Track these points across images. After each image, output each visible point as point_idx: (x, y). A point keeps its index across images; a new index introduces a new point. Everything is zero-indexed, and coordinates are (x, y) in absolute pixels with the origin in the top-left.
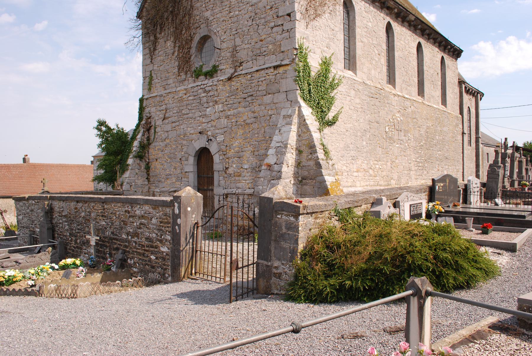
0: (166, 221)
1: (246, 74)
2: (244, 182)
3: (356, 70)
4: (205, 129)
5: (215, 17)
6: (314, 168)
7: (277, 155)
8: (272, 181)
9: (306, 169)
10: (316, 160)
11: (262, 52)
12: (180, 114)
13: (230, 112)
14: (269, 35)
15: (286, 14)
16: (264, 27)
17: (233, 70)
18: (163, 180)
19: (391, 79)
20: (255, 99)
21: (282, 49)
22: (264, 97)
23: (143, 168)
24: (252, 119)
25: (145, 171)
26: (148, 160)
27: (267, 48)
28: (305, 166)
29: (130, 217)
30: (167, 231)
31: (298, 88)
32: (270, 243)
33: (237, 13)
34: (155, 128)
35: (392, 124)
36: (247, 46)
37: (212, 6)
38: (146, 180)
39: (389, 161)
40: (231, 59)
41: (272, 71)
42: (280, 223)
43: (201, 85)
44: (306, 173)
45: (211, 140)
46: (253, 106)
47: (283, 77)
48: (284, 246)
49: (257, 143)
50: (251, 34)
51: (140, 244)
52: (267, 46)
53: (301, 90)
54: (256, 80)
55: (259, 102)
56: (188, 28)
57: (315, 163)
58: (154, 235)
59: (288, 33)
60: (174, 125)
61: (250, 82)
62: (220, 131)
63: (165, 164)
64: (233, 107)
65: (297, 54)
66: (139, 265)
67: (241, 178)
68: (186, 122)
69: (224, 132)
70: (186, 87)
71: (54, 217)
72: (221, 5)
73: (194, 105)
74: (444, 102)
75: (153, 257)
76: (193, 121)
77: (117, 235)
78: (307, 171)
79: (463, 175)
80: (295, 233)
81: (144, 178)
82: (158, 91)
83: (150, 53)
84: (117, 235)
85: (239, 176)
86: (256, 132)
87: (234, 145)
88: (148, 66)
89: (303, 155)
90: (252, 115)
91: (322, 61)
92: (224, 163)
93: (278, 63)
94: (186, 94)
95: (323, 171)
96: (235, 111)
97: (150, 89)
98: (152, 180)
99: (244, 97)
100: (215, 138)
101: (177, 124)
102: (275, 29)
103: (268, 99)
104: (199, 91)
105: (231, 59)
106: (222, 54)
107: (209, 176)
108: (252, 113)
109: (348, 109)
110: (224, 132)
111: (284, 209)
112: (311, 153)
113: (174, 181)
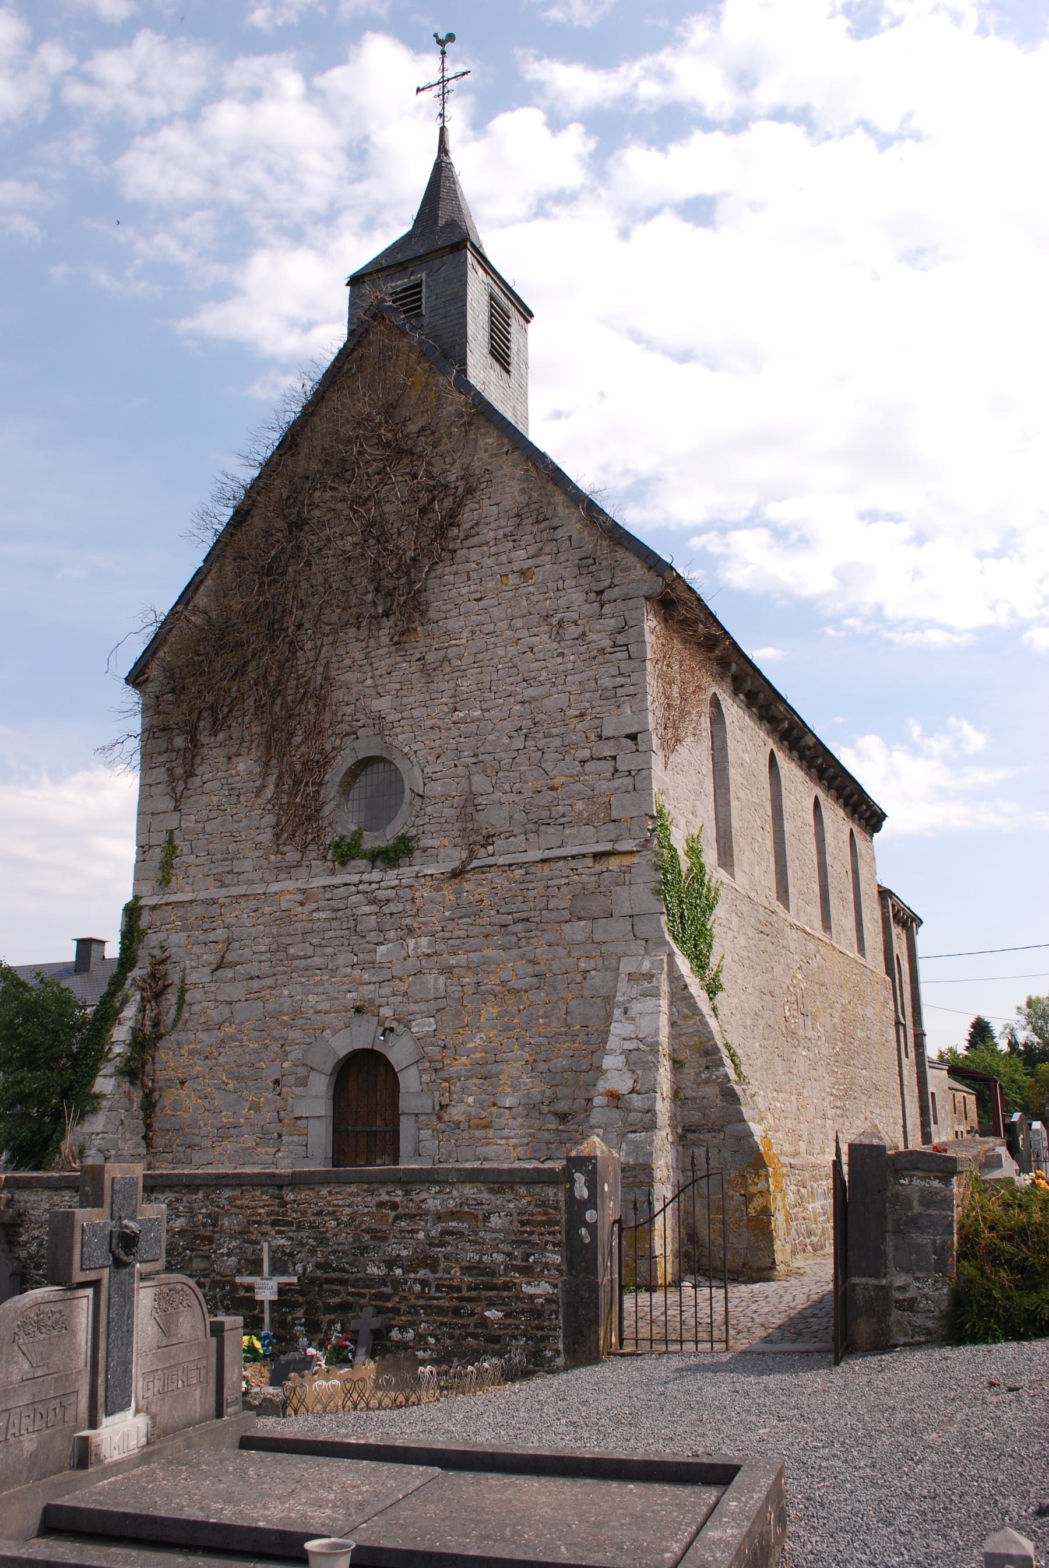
0: (544, 1218)
1: (510, 865)
2: (503, 1142)
3: (733, 865)
4: (372, 1001)
5: (406, 714)
6: (719, 1103)
7: (633, 1072)
8: (632, 1136)
9: (695, 1106)
10: (720, 1084)
11: (554, 814)
12: (280, 955)
13: (457, 957)
14: (576, 778)
15: (623, 733)
16: (561, 757)
17: (464, 854)
18: (207, 1143)
19: (783, 893)
20: (537, 929)
21: (615, 815)
22: (563, 926)
23: (135, 1106)
24: (528, 979)
25: (142, 1114)
26: (150, 1084)
27: (570, 808)
28: (693, 1099)
29: (397, 1218)
30: (546, 1243)
31: (665, 910)
32: (884, 1238)
33: (478, 713)
34: (183, 992)
35: (794, 998)
36: (510, 797)
37: (398, 686)
38: (143, 1142)
39: (794, 1092)
40: (458, 825)
41: (590, 865)
42: (907, 1197)
43: (361, 882)
44: (696, 1117)
45: (392, 1030)
46: (531, 947)
47: (621, 880)
48: (920, 1241)
49: (545, 1041)
50: (522, 768)
51: (444, 1286)
52: (570, 802)
53: (668, 915)
54: (543, 883)
55: (549, 936)
56: (315, 732)
57: (721, 1090)
58: (499, 1258)
59: (630, 779)
60: (255, 984)
61: (522, 886)
62: (423, 1006)
63: (217, 1094)
64: (467, 947)
65: (653, 830)
66: (437, 1340)
67: (491, 1133)
68: (303, 980)
69: (438, 1011)
70: (301, 884)
71: (24, 1238)
72: (425, 689)
73: (331, 934)
74: (861, 949)
75: (494, 1314)
76: (325, 978)
77: (343, 1270)
78: (698, 1110)
79: (905, 1133)
80: (944, 1213)
81: (138, 1134)
82: (196, 888)
83: (172, 779)
84: (343, 1270)
85: (487, 1127)
86: (541, 1013)
87: (471, 1045)
88: (161, 816)
89: (686, 1070)
90: (529, 969)
91: (688, 844)
92: (437, 1094)
93: (607, 847)
94: (302, 904)
95: (743, 1109)
96: (474, 957)
97: (164, 882)
98: (159, 1141)
99: (503, 923)
100: (405, 1026)
101: (269, 982)
102: (590, 766)
103: (577, 930)
104: (353, 899)
105: (458, 825)
106: (429, 810)
107: (374, 1129)
108: (530, 965)
109: (730, 960)
110: (438, 1011)
111: (919, 1165)
112: (707, 1068)
113: (250, 1143)
